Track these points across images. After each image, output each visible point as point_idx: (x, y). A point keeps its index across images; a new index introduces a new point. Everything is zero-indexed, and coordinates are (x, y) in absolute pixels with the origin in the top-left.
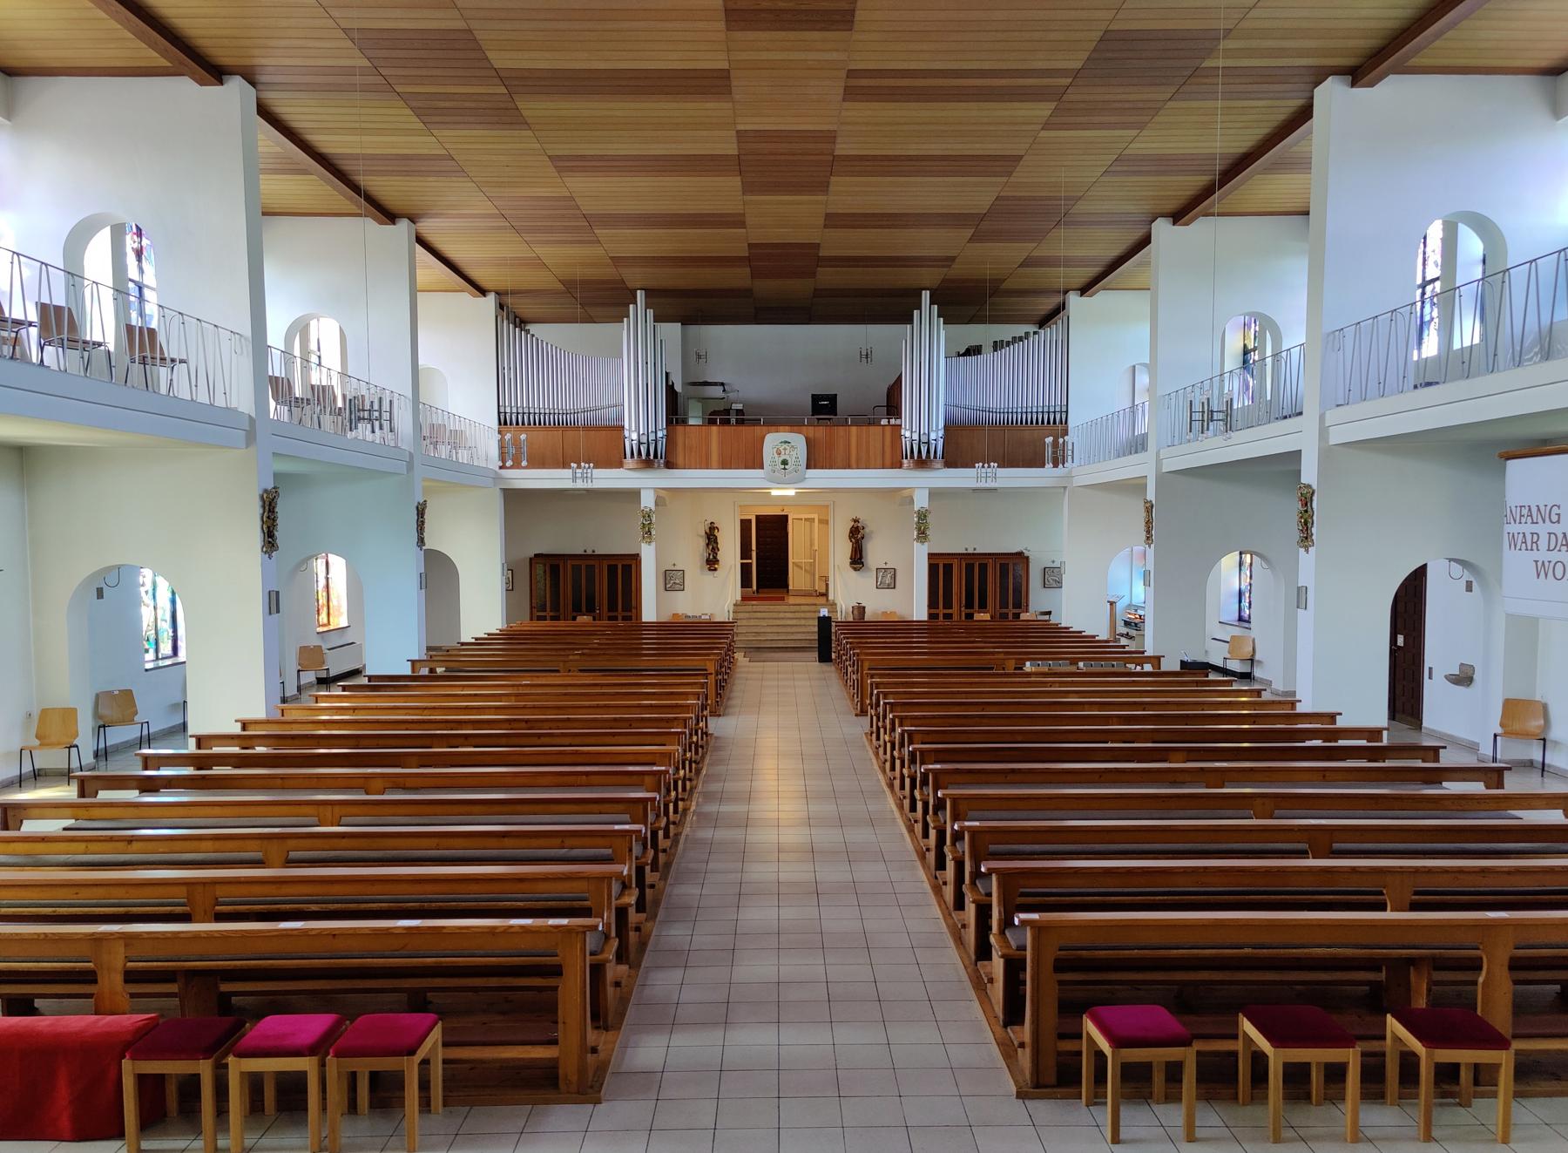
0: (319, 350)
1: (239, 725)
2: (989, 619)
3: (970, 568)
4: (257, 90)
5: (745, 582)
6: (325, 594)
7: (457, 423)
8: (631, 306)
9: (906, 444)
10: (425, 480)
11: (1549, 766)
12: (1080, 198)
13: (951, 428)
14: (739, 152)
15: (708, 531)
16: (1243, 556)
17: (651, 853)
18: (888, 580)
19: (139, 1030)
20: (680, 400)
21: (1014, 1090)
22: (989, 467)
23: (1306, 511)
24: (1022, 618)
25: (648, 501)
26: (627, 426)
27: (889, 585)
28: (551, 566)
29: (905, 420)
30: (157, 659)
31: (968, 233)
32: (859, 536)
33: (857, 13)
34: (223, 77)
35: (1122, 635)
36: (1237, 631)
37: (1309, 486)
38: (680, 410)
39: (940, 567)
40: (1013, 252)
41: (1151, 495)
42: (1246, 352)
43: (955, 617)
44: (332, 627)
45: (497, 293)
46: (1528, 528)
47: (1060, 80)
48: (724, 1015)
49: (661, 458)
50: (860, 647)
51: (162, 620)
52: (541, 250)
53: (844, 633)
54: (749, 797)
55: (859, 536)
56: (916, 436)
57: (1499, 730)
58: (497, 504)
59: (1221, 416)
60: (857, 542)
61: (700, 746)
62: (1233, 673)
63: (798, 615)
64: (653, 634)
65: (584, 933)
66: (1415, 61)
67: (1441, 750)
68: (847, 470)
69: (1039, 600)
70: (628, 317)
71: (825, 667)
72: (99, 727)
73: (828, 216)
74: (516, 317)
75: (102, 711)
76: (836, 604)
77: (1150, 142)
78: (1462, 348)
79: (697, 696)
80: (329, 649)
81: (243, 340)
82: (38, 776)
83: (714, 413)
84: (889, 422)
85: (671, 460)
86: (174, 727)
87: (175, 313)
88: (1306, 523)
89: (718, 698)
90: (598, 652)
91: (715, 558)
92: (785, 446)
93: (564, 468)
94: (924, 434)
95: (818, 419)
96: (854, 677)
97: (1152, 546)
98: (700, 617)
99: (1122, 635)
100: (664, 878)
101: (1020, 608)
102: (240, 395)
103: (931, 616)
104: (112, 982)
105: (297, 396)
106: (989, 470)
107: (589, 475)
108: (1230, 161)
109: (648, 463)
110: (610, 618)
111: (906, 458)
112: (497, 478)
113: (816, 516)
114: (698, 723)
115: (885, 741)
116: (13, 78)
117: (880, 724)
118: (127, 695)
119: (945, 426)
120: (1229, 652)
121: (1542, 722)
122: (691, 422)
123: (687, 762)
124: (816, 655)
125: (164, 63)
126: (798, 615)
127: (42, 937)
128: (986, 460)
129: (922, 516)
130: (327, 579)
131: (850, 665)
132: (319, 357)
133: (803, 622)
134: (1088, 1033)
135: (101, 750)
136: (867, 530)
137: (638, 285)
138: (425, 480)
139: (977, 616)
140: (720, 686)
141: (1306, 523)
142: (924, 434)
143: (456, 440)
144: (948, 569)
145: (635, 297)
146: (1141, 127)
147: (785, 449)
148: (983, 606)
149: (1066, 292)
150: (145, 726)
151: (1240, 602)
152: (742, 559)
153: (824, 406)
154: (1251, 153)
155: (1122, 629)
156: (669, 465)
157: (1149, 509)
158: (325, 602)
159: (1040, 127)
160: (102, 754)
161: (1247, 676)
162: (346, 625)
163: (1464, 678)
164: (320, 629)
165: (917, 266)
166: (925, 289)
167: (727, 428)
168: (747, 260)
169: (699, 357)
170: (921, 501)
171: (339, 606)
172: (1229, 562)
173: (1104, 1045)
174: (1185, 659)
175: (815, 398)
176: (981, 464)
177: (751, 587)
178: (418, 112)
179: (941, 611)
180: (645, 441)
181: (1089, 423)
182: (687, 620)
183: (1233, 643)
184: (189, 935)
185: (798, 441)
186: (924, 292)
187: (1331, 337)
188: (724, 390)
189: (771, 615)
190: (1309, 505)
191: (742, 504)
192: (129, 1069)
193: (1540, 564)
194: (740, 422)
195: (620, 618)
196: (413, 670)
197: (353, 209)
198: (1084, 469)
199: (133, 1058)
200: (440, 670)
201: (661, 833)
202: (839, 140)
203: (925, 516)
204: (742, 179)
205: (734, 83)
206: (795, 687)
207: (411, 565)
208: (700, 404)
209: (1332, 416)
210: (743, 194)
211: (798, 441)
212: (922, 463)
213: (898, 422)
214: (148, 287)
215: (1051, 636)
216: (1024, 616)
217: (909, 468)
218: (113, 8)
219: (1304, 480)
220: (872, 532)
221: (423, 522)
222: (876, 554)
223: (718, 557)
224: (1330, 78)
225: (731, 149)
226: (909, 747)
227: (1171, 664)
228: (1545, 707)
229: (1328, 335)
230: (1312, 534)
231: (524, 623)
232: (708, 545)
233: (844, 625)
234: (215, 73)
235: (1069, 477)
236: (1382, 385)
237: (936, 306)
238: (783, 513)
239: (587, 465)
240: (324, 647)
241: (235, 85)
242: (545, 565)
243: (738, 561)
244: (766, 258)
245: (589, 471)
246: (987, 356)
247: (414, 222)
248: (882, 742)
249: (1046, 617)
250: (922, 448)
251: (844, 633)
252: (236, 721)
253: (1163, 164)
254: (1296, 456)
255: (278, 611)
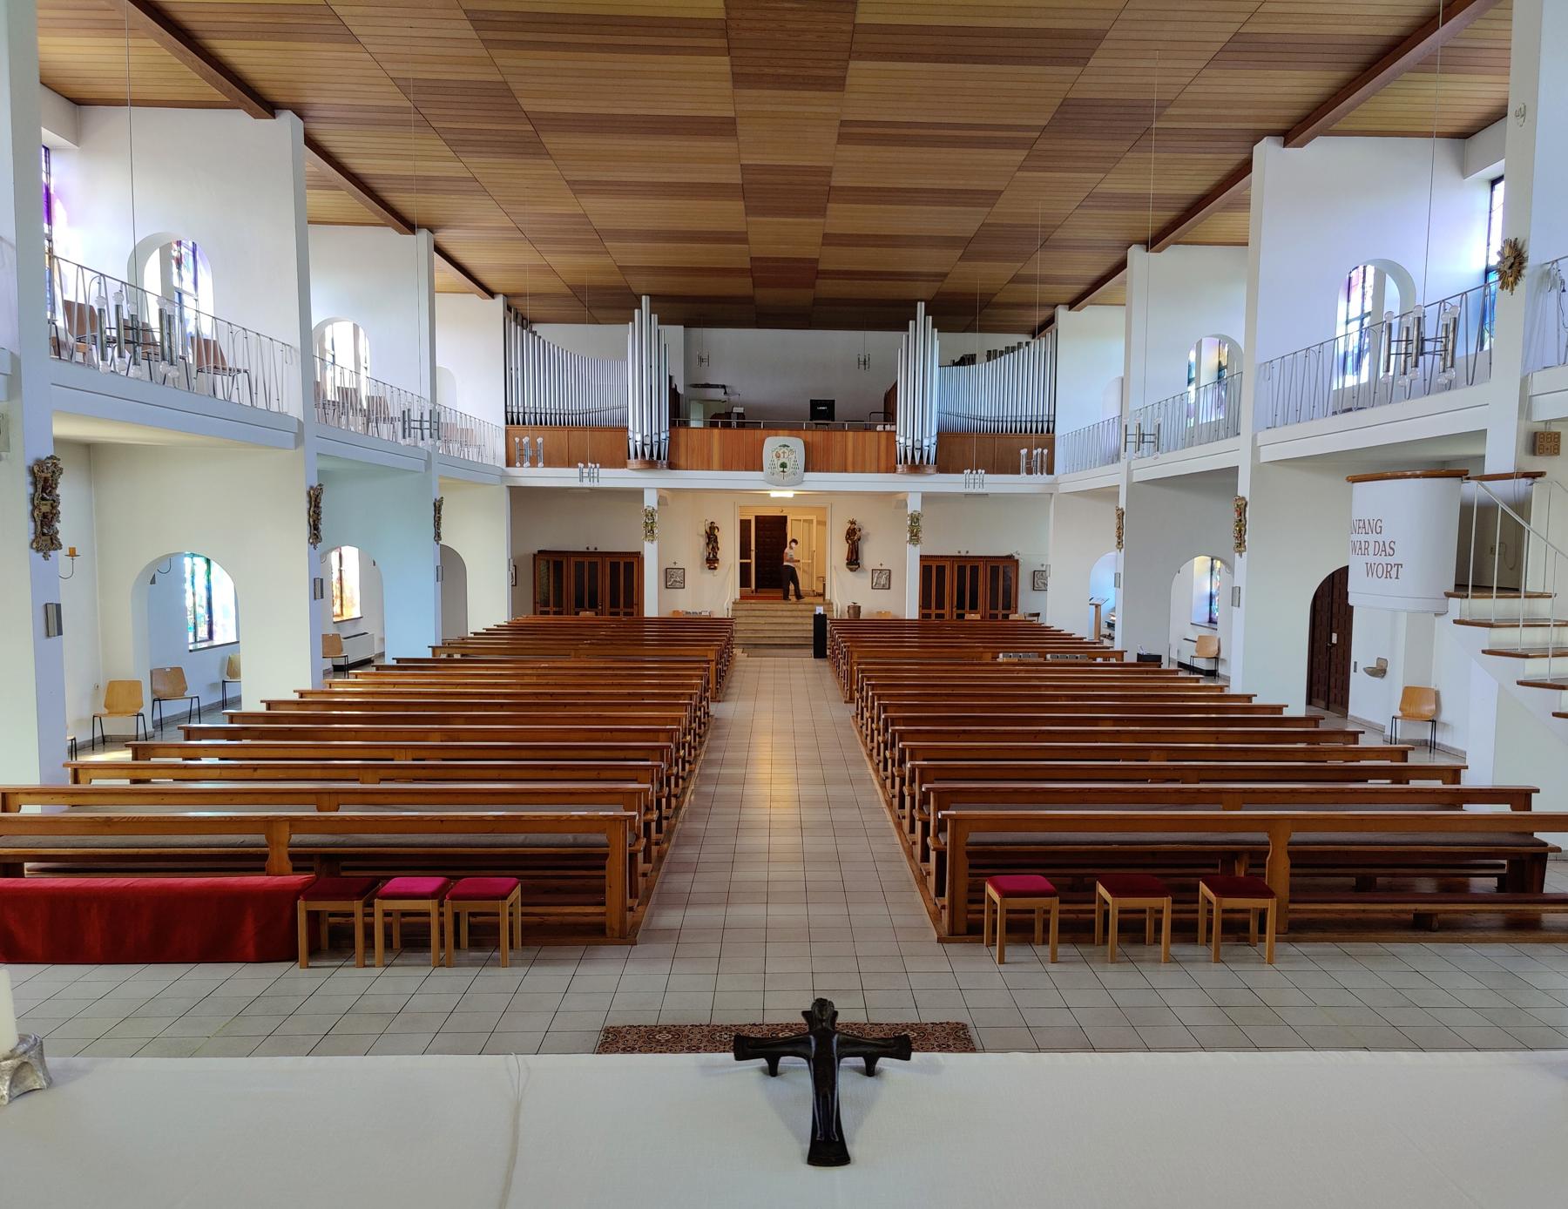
0: (333, 349)
1: (297, 695)
2: (979, 618)
3: (962, 570)
4: (304, 122)
5: (744, 582)
6: (338, 586)
7: (458, 417)
8: (636, 311)
9: (900, 449)
10: (441, 477)
11: (1439, 744)
12: (1059, 226)
13: (944, 436)
14: (727, 13)
15: (708, 531)
16: (1214, 561)
17: (643, 841)
18: (883, 581)
19: (304, 884)
20: (682, 402)
21: (936, 936)
22: (977, 473)
23: (1240, 520)
24: (1010, 618)
25: (650, 501)
26: (631, 427)
27: (884, 585)
28: (554, 562)
29: (900, 426)
30: (196, 641)
31: (959, 253)
32: (856, 538)
33: (847, 79)
34: (276, 111)
35: (1105, 636)
36: (1205, 632)
37: (1243, 498)
38: (682, 410)
39: (932, 570)
40: (1003, 270)
41: (1122, 504)
42: (1220, 368)
43: (947, 617)
44: (345, 618)
45: (505, 295)
46: (1363, 537)
47: (1029, 133)
48: (727, 899)
49: (664, 459)
50: (851, 641)
51: (200, 606)
52: (551, 259)
53: (843, 637)
54: (746, 763)
55: (856, 538)
56: (909, 443)
57: (1399, 714)
58: (504, 499)
59: (1152, 438)
60: (854, 543)
61: (702, 726)
62: (1200, 671)
63: (795, 614)
64: (655, 627)
65: (626, 821)
66: (1336, 127)
67: (1533, 794)
68: (844, 474)
69: (1027, 602)
70: (633, 321)
71: (820, 662)
72: (154, 700)
73: (825, 236)
74: (523, 319)
75: (155, 687)
76: (832, 604)
77: (1115, 184)
78: (1338, 389)
79: (701, 677)
80: (345, 638)
81: (293, 351)
82: (105, 742)
83: (716, 416)
84: (884, 428)
85: (673, 461)
86: (213, 705)
87: (239, 329)
88: (1240, 531)
89: (718, 683)
90: (606, 642)
91: (715, 556)
92: (785, 449)
93: (569, 466)
94: (918, 440)
95: (816, 424)
96: (845, 668)
97: (1123, 550)
98: (701, 613)
99: (1105, 636)
100: (657, 869)
101: (1010, 609)
102: (292, 403)
103: (924, 616)
104: (280, 857)
105: (329, 398)
106: (977, 476)
107: (596, 475)
108: (1191, 201)
109: (651, 464)
110: (612, 614)
111: (901, 463)
112: (504, 476)
113: (814, 518)
114: (701, 702)
115: (878, 741)
116: (82, 107)
117: (874, 726)
118: (178, 672)
119: (938, 433)
120: (1197, 651)
121: (1433, 707)
122: (693, 424)
123: (680, 761)
124: (812, 651)
125: (223, 98)
126: (795, 614)
127: (228, 819)
128: (975, 467)
129: (915, 519)
130: (341, 571)
131: (857, 690)
132: (333, 356)
133: (800, 620)
134: (988, 894)
135: (99, 738)
136: (863, 532)
137: (644, 291)
138: (441, 477)
139: (968, 617)
140: (720, 675)
141: (1240, 531)
142: (918, 440)
143: (466, 437)
144: (941, 570)
145: (640, 301)
146: (1107, 171)
147: (784, 453)
148: (974, 607)
149: (1056, 306)
150: (195, 700)
151: (1211, 605)
152: (741, 558)
153: (822, 412)
154: (1207, 195)
155: (1105, 631)
156: (672, 466)
157: (1121, 515)
158: (339, 594)
159: (1016, 169)
160: (160, 724)
161: (1212, 674)
162: (359, 616)
163: (1379, 671)
164: (335, 619)
165: (913, 280)
166: (921, 301)
167: (728, 431)
168: (750, 272)
169: (701, 360)
170: (914, 505)
171: (352, 598)
172: (1201, 563)
173: (996, 897)
174: (1141, 652)
175: (814, 404)
176: (969, 471)
177: (750, 586)
178: (447, 142)
179: (934, 611)
180: (649, 442)
181: (1106, 422)
182: (688, 616)
183: (1201, 642)
184: (337, 819)
185: (796, 445)
186: (919, 303)
187: (1263, 368)
188: (725, 393)
189: (768, 613)
190: (1243, 514)
191: (742, 504)
192: (302, 906)
193: (1369, 565)
194: (741, 426)
195: (622, 613)
196: (434, 654)
197: (377, 219)
198: (1070, 476)
199: (305, 899)
200: (457, 656)
201: (640, 856)
202: (833, 174)
203: (917, 519)
204: (732, 61)
205: (739, 127)
206: (790, 672)
207: (428, 560)
208: (701, 406)
209: (1263, 437)
210: (746, 214)
211: (796, 445)
212: (916, 468)
213: (893, 428)
214: (186, 293)
215: (1036, 634)
216: (1012, 617)
217: (902, 473)
218: (189, 58)
219: (1240, 494)
220: (868, 534)
221: (439, 518)
222: (871, 555)
223: (718, 557)
224: (1265, 138)
225: (736, 178)
226: (920, 787)
227: (1130, 658)
228: (1437, 694)
229: (1261, 366)
230: (1245, 541)
231: (528, 616)
232: (708, 544)
233: (839, 622)
234: (269, 107)
235: (1055, 484)
236: (1356, 399)
237: (931, 317)
238: (782, 514)
239: (593, 466)
240: (342, 635)
241: (287, 119)
242: (548, 562)
243: (738, 561)
244: (766, 270)
245: (596, 470)
246: (980, 367)
247: (432, 232)
248: (865, 721)
249: (1036, 618)
250: (915, 453)
251: (843, 637)
252: (262, 702)
253: (1135, 202)
254: (1233, 471)
255: (322, 597)
